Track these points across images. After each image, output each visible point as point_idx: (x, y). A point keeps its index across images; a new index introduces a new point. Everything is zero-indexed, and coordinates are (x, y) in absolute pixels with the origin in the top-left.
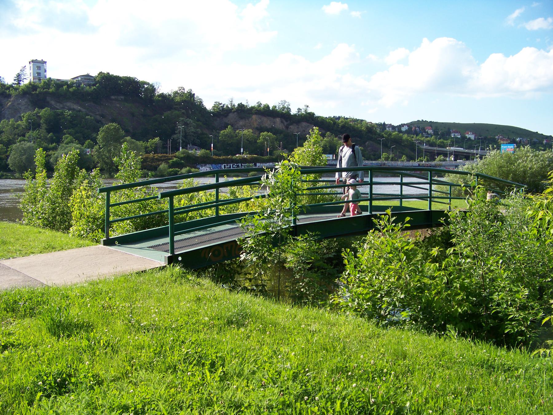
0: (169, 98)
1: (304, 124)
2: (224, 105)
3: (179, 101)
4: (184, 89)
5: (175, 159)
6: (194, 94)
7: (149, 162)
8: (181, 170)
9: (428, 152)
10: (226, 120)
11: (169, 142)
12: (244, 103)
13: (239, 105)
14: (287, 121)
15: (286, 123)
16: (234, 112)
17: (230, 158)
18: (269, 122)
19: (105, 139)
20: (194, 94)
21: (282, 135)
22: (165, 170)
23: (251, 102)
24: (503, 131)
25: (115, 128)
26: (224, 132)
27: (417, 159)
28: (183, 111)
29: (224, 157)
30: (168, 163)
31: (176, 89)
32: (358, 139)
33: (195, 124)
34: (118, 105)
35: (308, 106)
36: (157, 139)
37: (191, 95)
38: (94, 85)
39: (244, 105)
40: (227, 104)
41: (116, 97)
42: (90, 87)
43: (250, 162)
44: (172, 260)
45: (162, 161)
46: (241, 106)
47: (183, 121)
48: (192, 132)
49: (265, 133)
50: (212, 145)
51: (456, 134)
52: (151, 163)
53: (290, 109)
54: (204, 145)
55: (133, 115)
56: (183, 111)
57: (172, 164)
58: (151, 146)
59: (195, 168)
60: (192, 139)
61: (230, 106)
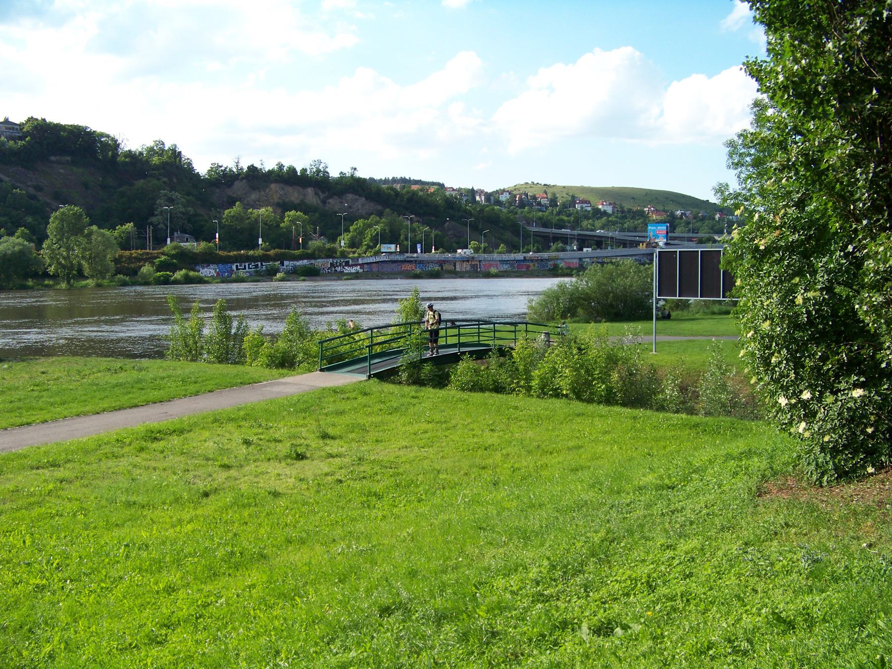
0: (142, 159)
1: (350, 196)
2: (226, 168)
3: (157, 163)
4: (163, 144)
5: (163, 258)
6: (180, 153)
7: (124, 262)
8: (174, 273)
9: (539, 236)
10: (229, 192)
11: (149, 231)
12: (258, 165)
13: (249, 167)
14: (323, 192)
15: (322, 196)
16: (243, 179)
17: (244, 254)
18: (296, 194)
19: (60, 231)
20: (180, 153)
21: (317, 215)
22: (150, 274)
23: (269, 165)
24: (656, 198)
25: (74, 214)
26: (230, 213)
27: (523, 248)
28: (165, 179)
29: (235, 253)
30: (154, 263)
31: (150, 144)
32: (433, 218)
33: (184, 201)
34: (62, 171)
35: (355, 169)
36: (129, 226)
37: (176, 154)
38: (21, 138)
39: (256, 168)
40: (230, 166)
41: (58, 158)
42: (16, 143)
43: (275, 260)
44: (370, 377)
45: (146, 260)
46: (252, 169)
47: (165, 195)
48: (181, 212)
49: (292, 213)
50: (217, 235)
51: (584, 205)
52: (128, 264)
53: (327, 173)
54: (199, 234)
55: (86, 186)
56: (165, 179)
57: (159, 265)
58: (120, 236)
59: (194, 270)
60: (181, 224)
61: (235, 170)
